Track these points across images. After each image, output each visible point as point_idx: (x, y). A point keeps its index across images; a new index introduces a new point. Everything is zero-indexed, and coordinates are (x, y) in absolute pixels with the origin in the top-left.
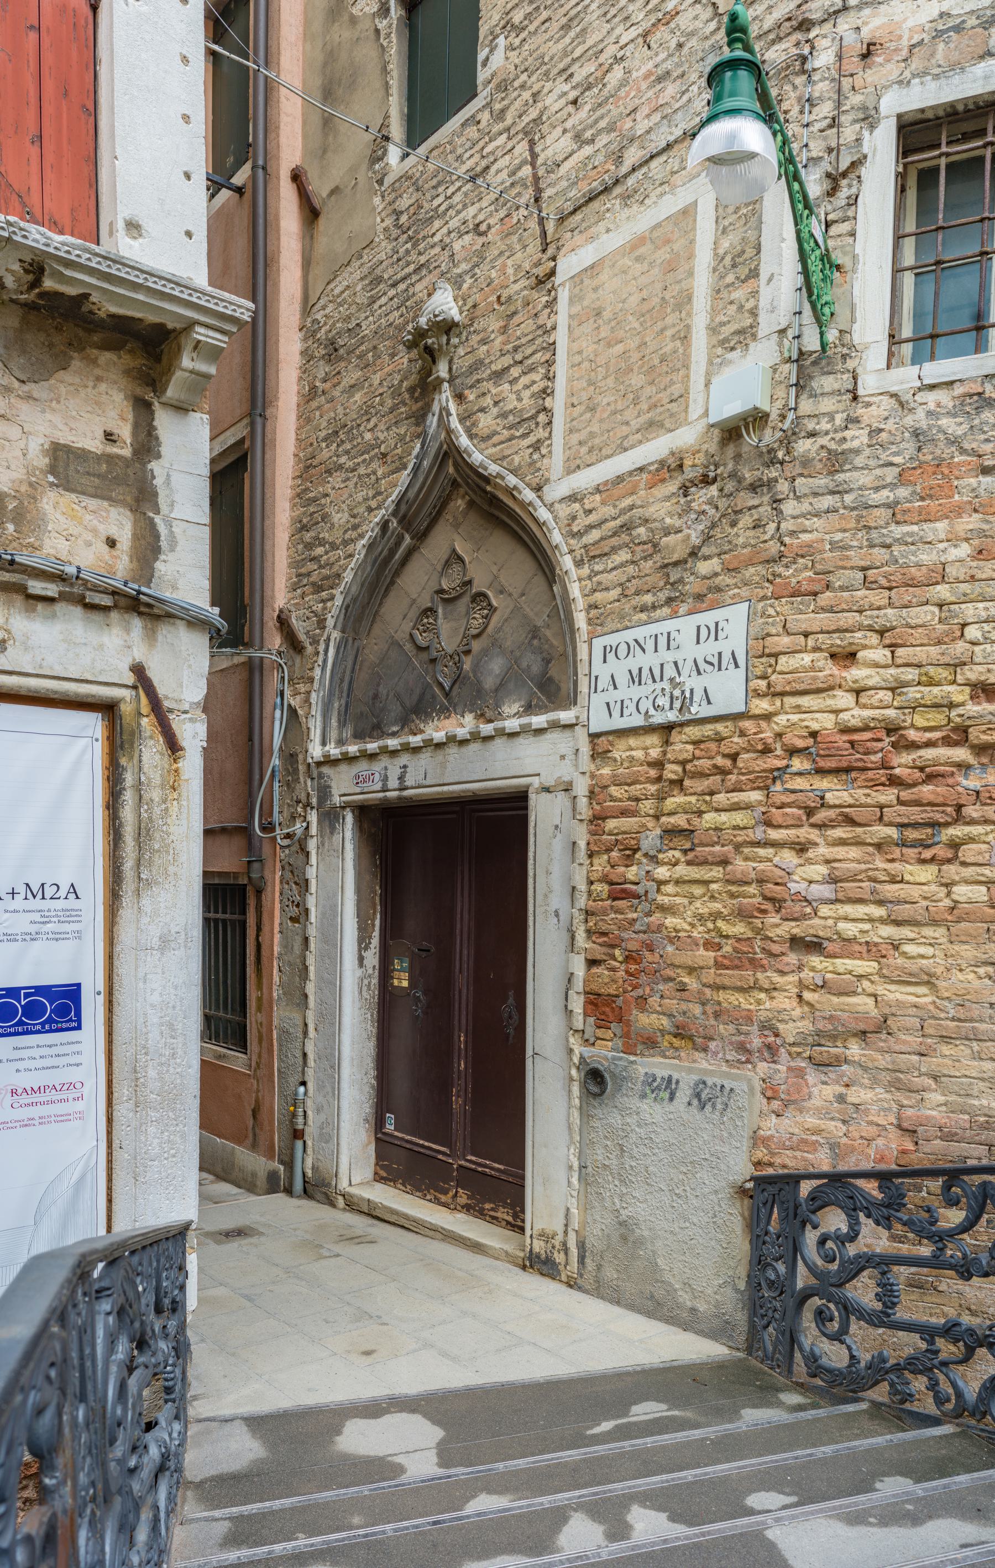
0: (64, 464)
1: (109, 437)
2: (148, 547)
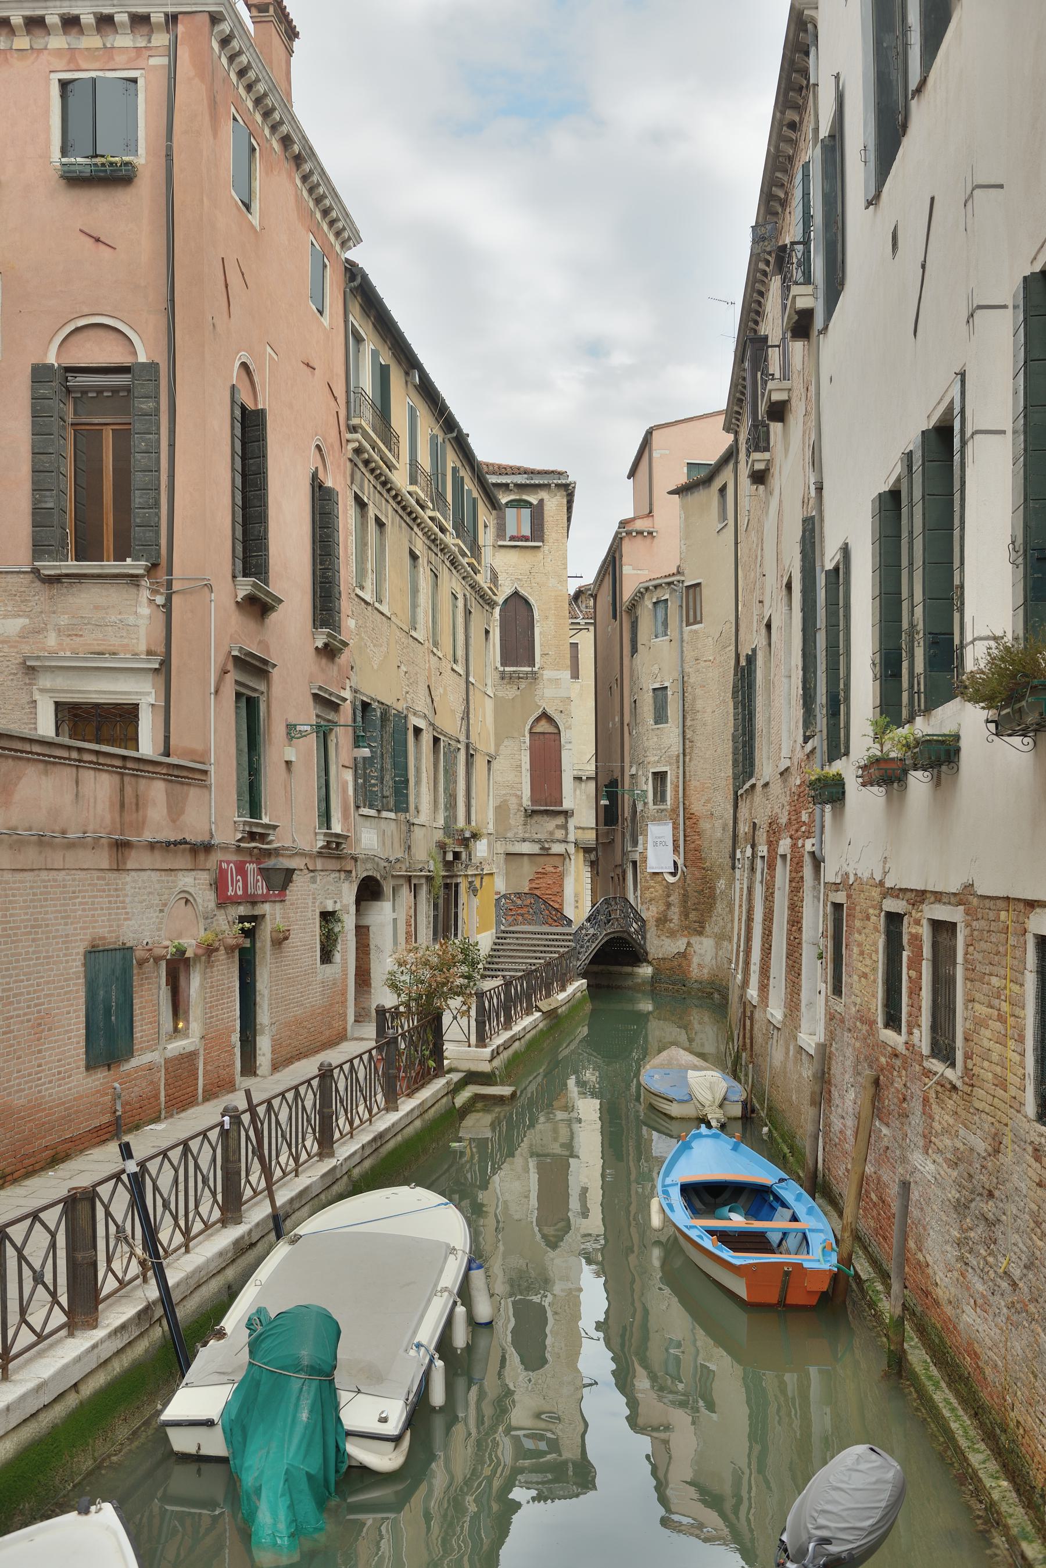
0: (558, 827)
1: (701, 943)
2: (567, 834)
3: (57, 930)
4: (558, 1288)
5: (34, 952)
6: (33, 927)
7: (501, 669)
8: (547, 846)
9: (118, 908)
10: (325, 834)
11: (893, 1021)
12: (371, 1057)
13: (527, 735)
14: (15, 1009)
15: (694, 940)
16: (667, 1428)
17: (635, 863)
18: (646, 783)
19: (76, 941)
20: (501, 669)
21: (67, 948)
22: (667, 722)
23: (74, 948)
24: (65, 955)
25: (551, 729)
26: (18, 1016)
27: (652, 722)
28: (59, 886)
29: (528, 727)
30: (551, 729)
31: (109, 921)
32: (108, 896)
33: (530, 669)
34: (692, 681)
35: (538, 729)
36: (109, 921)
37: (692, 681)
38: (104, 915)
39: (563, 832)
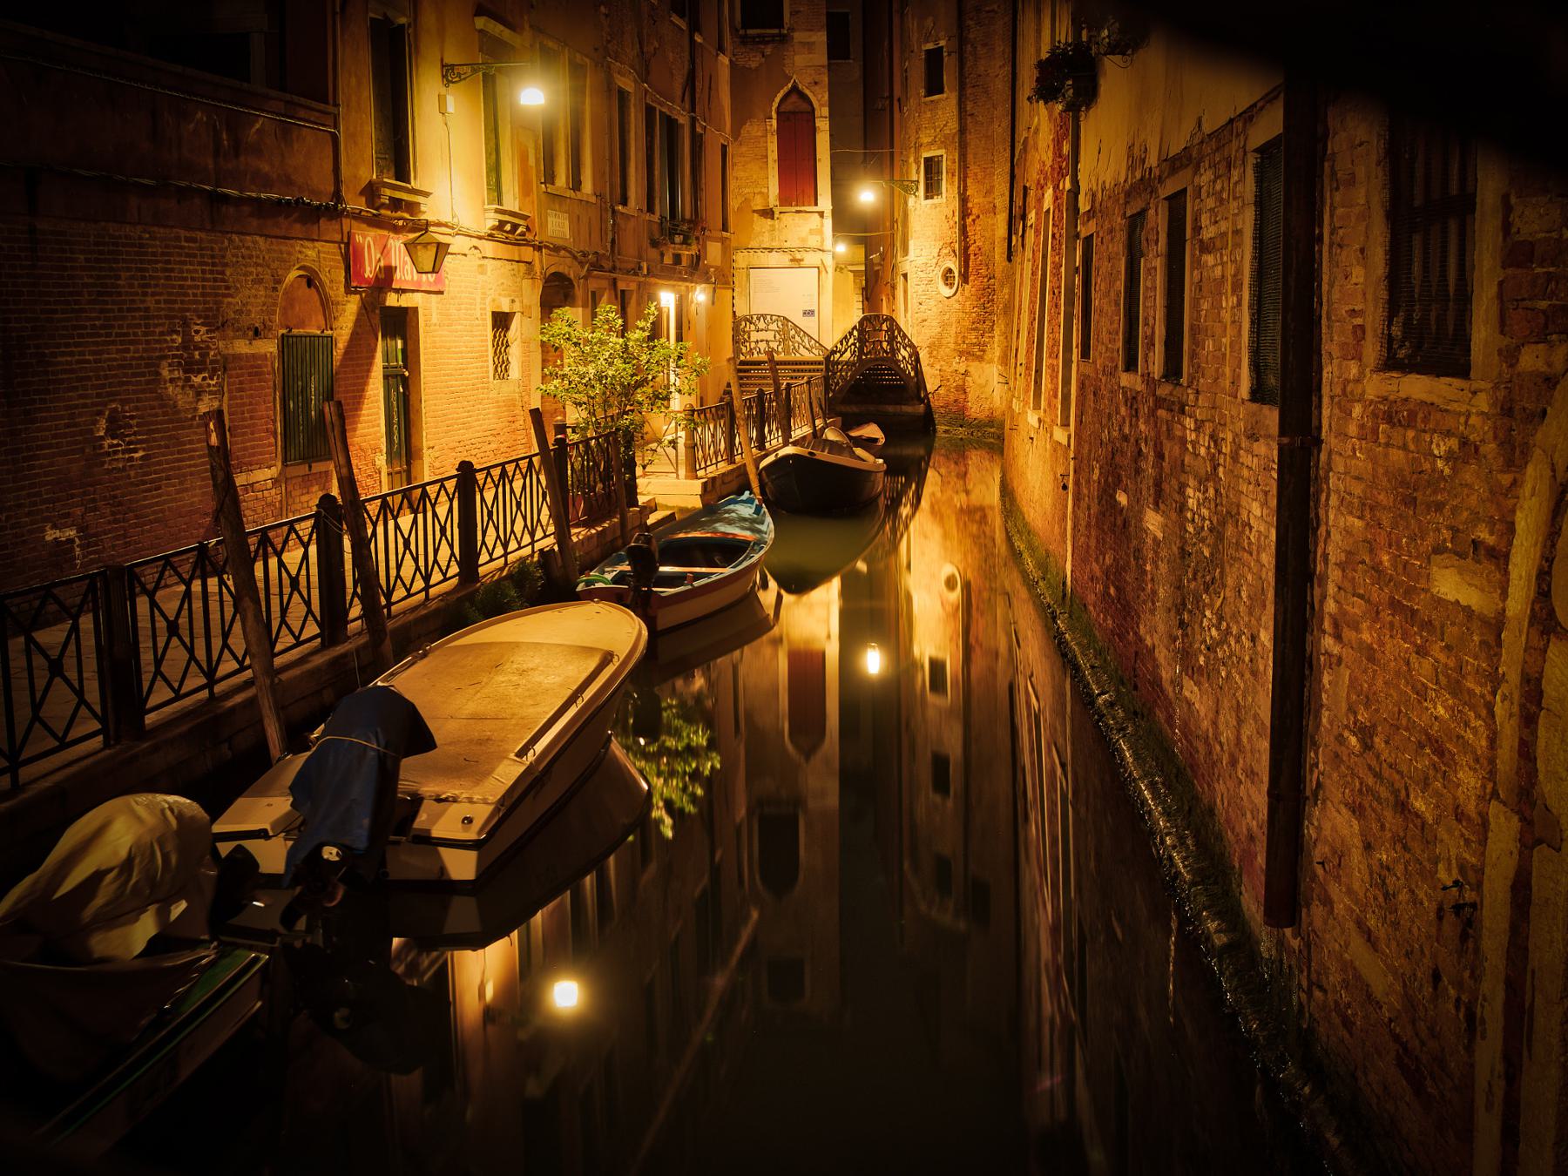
0: (811, 232)
2: (823, 240)
3: (133, 301)
4: (255, 222)
5: (103, 327)
6: (99, 294)
7: (742, 32)
8: (798, 256)
9: (215, 280)
10: (497, 211)
11: (1130, 365)
12: (531, 464)
13: (774, 115)
14: (81, 396)
15: (974, 367)
16: (466, 472)
17: (905, 276)
18: (918, 172)
19: (159, 317)
20: (742, 32)
21: (147, 325)
22: (942, 92)
23: (156, 326)
24: (145, 334)
25: (805, 107)
26: (85, 406)
27: (922, 92)
28: (133, 245)
29: (775, 105)
30: (805, 107)
31: (203, 295)
32: (200, 264)
33: (776, 31)
34: (971, 36)
35: (788, 107)
36: (203, 295)
37: (971, 36)
38: (197, 287)
39: (818, 238)
